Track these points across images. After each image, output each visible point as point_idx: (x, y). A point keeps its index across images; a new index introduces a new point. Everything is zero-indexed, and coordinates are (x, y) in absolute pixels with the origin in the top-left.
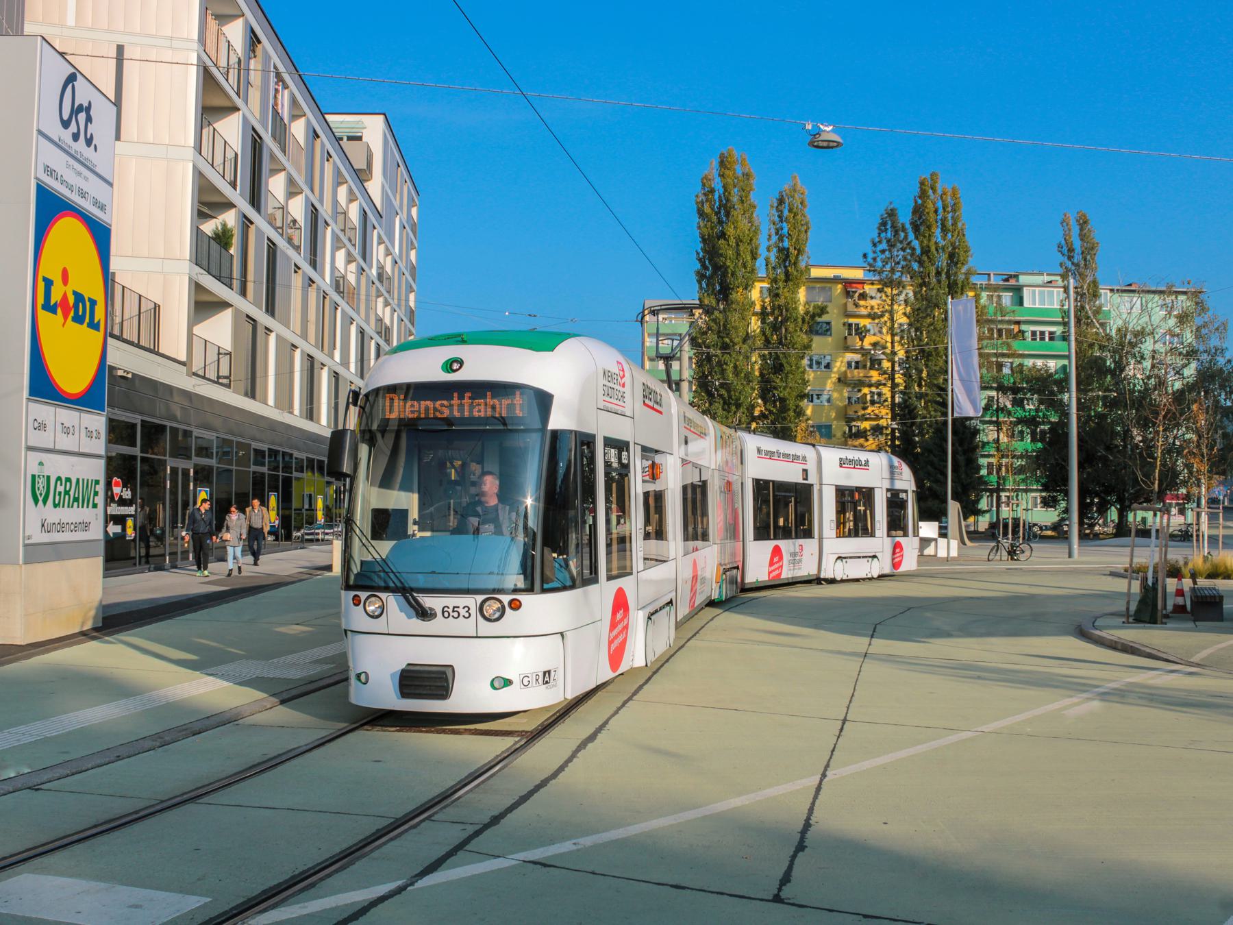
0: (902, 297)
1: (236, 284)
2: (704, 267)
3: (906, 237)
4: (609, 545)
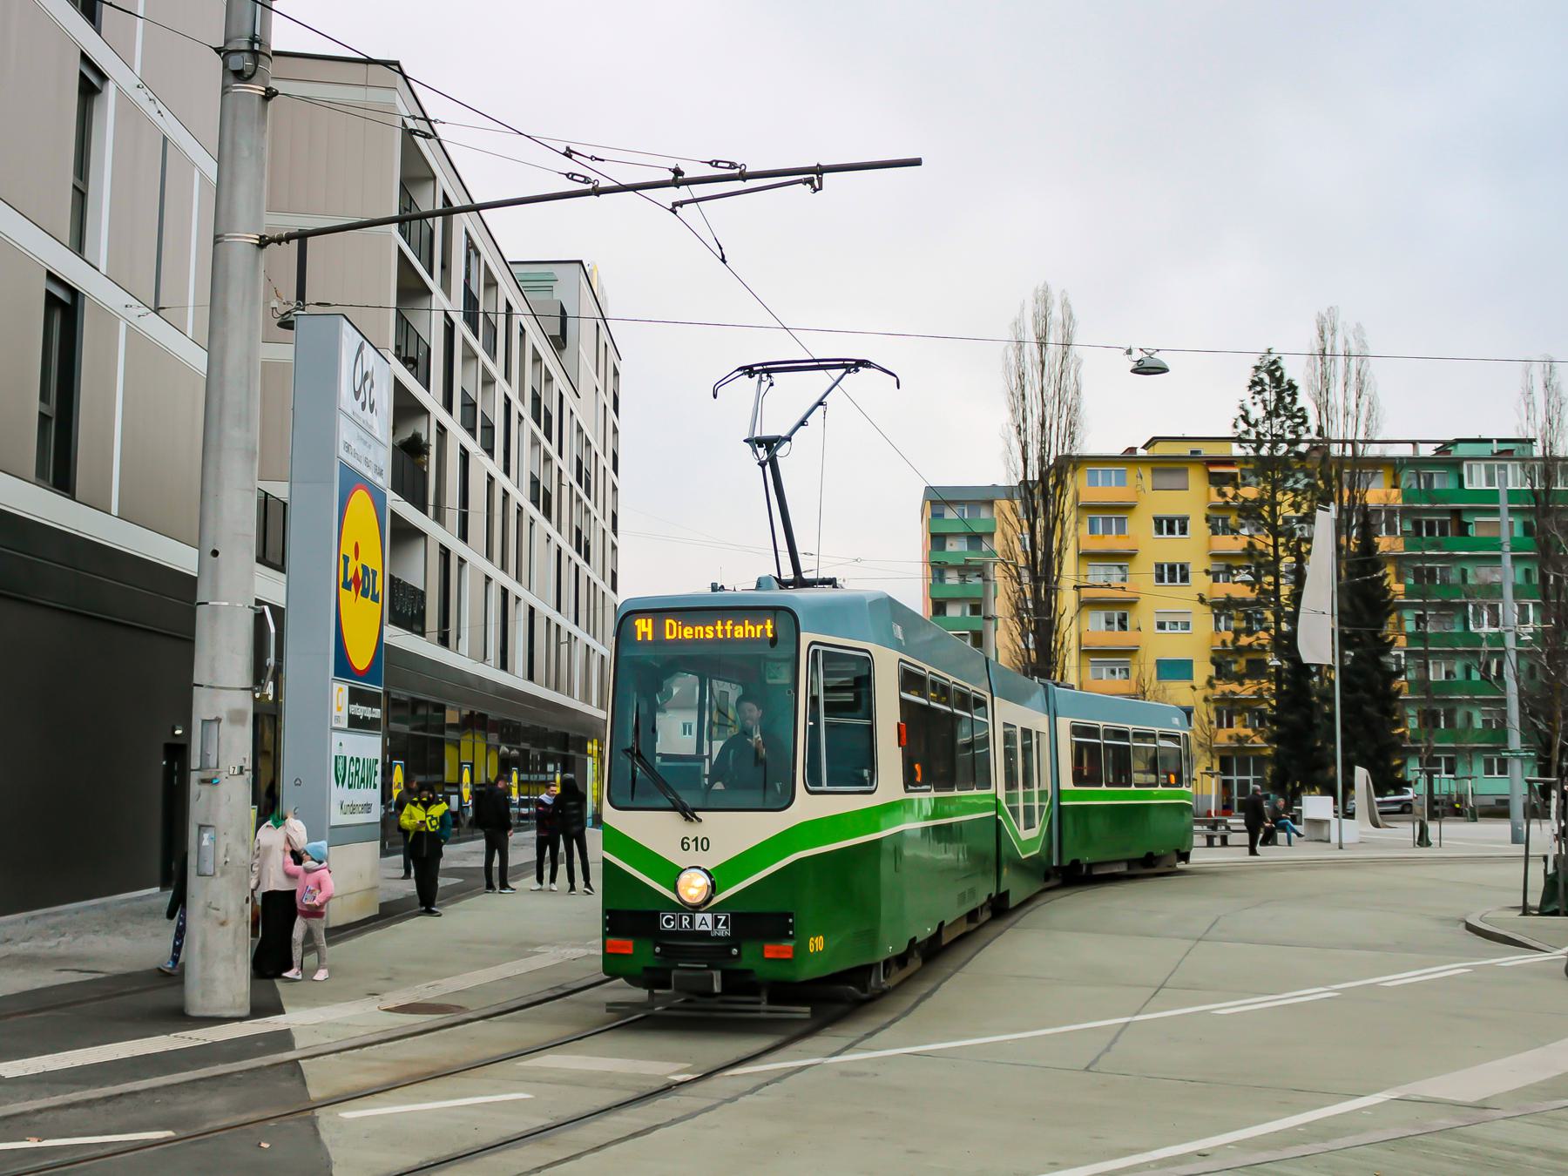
1: (431, 510)
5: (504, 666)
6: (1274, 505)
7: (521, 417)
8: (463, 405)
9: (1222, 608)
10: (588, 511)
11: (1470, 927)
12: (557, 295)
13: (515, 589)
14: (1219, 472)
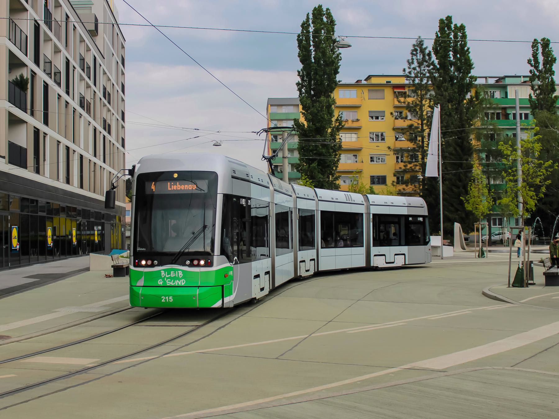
0: (428, 96)
1: (29, 111)
2: (302, 80)
3: (430, 58)
4: (214, 225)
5: (68, 182)
6: (421, 106)
7: (74, 67)
8: (45, 62)
9: (399, 152)
10: (109, 110)
11: (484, 294)
12: (93, 11)
13: (72, 146)
14: (398, 90)
